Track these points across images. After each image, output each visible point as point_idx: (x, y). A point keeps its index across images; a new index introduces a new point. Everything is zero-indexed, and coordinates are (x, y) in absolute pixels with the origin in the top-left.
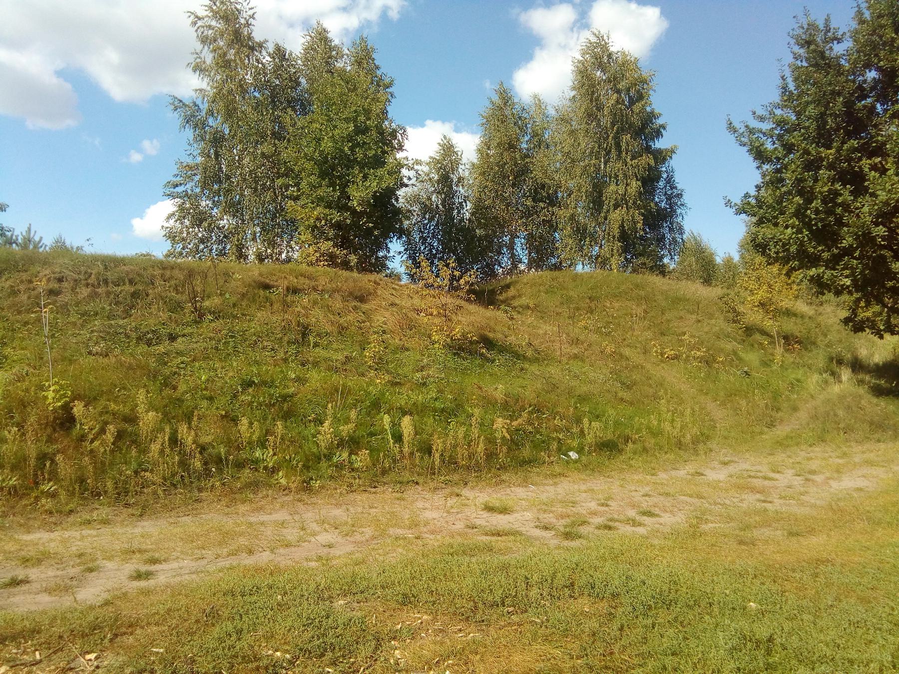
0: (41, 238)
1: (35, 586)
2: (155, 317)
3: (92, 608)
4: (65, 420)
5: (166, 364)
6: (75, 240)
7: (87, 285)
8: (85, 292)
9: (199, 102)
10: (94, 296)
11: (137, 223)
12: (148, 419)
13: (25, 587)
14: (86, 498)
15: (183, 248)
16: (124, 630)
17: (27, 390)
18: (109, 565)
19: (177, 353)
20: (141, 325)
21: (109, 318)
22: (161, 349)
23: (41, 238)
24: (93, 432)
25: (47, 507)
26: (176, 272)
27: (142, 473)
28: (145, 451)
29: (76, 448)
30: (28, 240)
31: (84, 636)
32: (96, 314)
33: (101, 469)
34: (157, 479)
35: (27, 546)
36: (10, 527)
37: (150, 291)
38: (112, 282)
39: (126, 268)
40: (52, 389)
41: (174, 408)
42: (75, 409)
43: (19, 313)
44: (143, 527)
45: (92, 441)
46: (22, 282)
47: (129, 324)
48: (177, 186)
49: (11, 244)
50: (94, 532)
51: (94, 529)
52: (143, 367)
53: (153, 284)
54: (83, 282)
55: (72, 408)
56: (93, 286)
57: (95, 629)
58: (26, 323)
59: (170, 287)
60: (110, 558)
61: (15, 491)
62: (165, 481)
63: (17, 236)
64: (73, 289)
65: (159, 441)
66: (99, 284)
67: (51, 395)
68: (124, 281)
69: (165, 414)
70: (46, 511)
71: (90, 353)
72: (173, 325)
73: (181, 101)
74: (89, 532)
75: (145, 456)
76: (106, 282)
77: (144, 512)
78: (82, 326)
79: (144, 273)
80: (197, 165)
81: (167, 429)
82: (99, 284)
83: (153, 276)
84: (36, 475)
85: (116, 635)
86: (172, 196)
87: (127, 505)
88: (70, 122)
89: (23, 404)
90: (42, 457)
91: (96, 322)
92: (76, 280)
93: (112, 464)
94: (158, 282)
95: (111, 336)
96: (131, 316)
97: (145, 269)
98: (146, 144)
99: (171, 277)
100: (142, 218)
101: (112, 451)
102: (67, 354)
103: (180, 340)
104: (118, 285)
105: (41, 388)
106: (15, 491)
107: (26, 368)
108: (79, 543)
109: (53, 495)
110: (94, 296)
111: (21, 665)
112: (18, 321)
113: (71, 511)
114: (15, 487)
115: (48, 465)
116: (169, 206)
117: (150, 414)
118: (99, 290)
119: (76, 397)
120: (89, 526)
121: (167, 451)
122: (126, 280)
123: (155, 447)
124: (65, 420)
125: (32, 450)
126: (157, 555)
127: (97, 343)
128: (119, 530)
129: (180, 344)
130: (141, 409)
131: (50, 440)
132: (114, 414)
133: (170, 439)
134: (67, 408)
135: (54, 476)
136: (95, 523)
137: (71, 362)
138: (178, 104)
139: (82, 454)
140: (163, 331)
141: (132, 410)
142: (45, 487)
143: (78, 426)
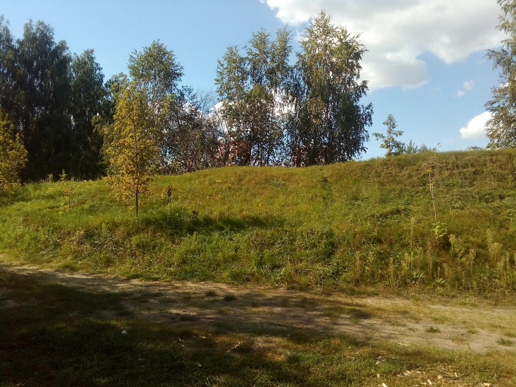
0: (417, 146)
1: (444, 335)
2: (489, 185)
3: (480, 355)
4: (445, 245)
5: (499, 213)
6: (430, 146)
7: (447, 169)
8: (446, 173)
9: (505, 48)
10: (451, 175)
11: (463, 131)
12: (494, 247)
13: (438, 334)
14: (461, 290)
15: (498, 141)
16: (505, 374)
17: (423, 228)
18: (482, 332)
19: (506, 207)
20: (481, 190)
21: (461, 187)
22: (495, 204)
23: (417, 146)
24: (461, 252)
25: (440, 292)
26: (500, 157)
27: (494, 280)
28: (493, 266)
29: (453, 261)
30: (410, 148)
31: (480, 371)
32: (454, 185)
33: (468, 275)
34: (503, 283)
35: (434, 312)
36: (423, 300)
37: (485, 170)
38: (462, 167)
39: (469, 158)
40: (437, 227)
41: (509, 241)
42: (451, 239)
43: (414, 187)
44: (498, 312)
45: (461, 258)
46: (413, 170)
47: (474, 190)
48: (493, 103)
49: (402, 151)
50: (469, 311)
51: (468, 308)
52: (486, 216)
53: (485, 165)
54: (445, 168)
55: (449, 239)
56: (451, 170)
57: (486, 369)
58: (418, 192)
59: (497, 166)
60: (483, 328)
61: (423, 281)
62: (509, 285)
63: (405, 147)
64: (440, 172)
65: (503, 261)
66: (454, 168)
67: (436, 231)
68: (468, 165)
69: (504, 244)
70: (440, 294)
71: (454, 208)
72: (501, 190)
73: (493, 51)
74: (467, 310)
75: (493, 269)
76: (457, 167)
77: (497, 303)
78: (447, 192)
79: (479, 159)
80: (505, 88)
81: (508, 254)
82: (454, 168)
83: (485, 161)
84: (433, 274)
85: (500, 376)
86: (493, 110)
87: (486, 297)
88: (425, 82)
89: (423, 235)
90: (436, 264)
91: (455, 190)
92: (441, 167)
93: (474, 272)
94: (489, 164)
95: (462, 197)
96: (474, 185)
97: (480, 157)
98: (466, 84)
99: (497, 160)
100: (466, 128)
101: (474, 265)
102: (441, 208)
103: (507, 199)
104: (465, 168)
105: (430, 226)
106: (423, 281)
107: (421, 216)
108: (462, 315)
109: (443, 286)
110: (451, 175)
111: (449, 377)
112: (413, 191)
113: (454, 296)
114: (423, 278)
115: (439, 269)
116: (488, 116)
117: (495, 244)
118: (454, 172)
119: (449, 233)
120: (465, 306)
121: (508, 267)
122: (470, 164)
123: (500, 265)
124: (445, 245)
125: (430, 259)
126: (512, 332)
127: (456, 202)
128: (482, 311)
129: (507, 201)
130: (490, 240)
131: (438, 256)
132: (472, 243)
133: (510, 261)
134: (446, 238)
135: (442, 275)
136: (468, 305)
137: (444, 213)
138: (492, 53)
139: (457, 264)
140: (495, 194)
141: (483, 241)
142: (439, 281)
143: (452, 249)
